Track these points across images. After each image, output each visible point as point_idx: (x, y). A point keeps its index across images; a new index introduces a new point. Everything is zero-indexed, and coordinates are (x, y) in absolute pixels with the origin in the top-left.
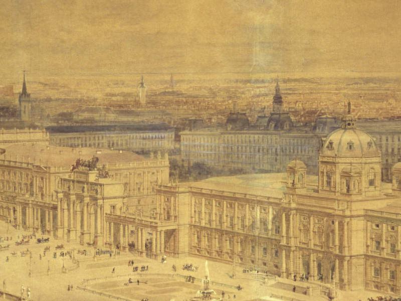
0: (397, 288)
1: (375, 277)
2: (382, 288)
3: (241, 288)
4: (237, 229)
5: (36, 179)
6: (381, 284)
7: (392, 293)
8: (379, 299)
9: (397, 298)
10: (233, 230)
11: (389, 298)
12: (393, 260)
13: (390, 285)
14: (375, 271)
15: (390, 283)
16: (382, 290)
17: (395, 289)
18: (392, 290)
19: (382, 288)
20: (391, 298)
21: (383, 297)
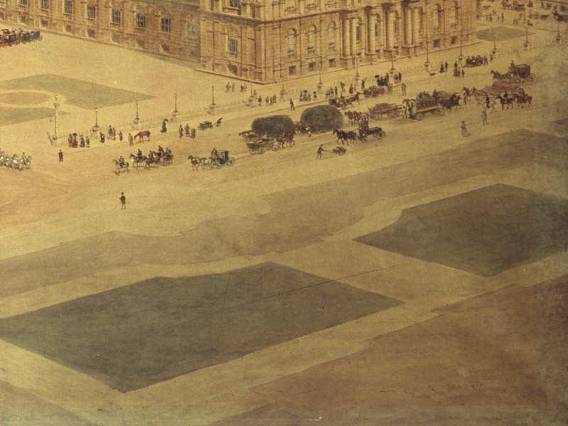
0: (31, 17)
1: (21, 6)
2: (8, 17)
3: (400, 75)
4: (221, 10)
5: (351, 24)
6: (7, 11)
7: (23, 24)
8: (4, 32)
9: (30, 31)
10: (239, 14)
11: (19, 31)
12: (235, 18)
13: (19, 12)
14: (113, 14)
15: (19, 10)
16: (9, 21)
17: (26, 18)
18: (23, 19)
19: (8, 17)
20: (22, 31)
21: (10, 30)
